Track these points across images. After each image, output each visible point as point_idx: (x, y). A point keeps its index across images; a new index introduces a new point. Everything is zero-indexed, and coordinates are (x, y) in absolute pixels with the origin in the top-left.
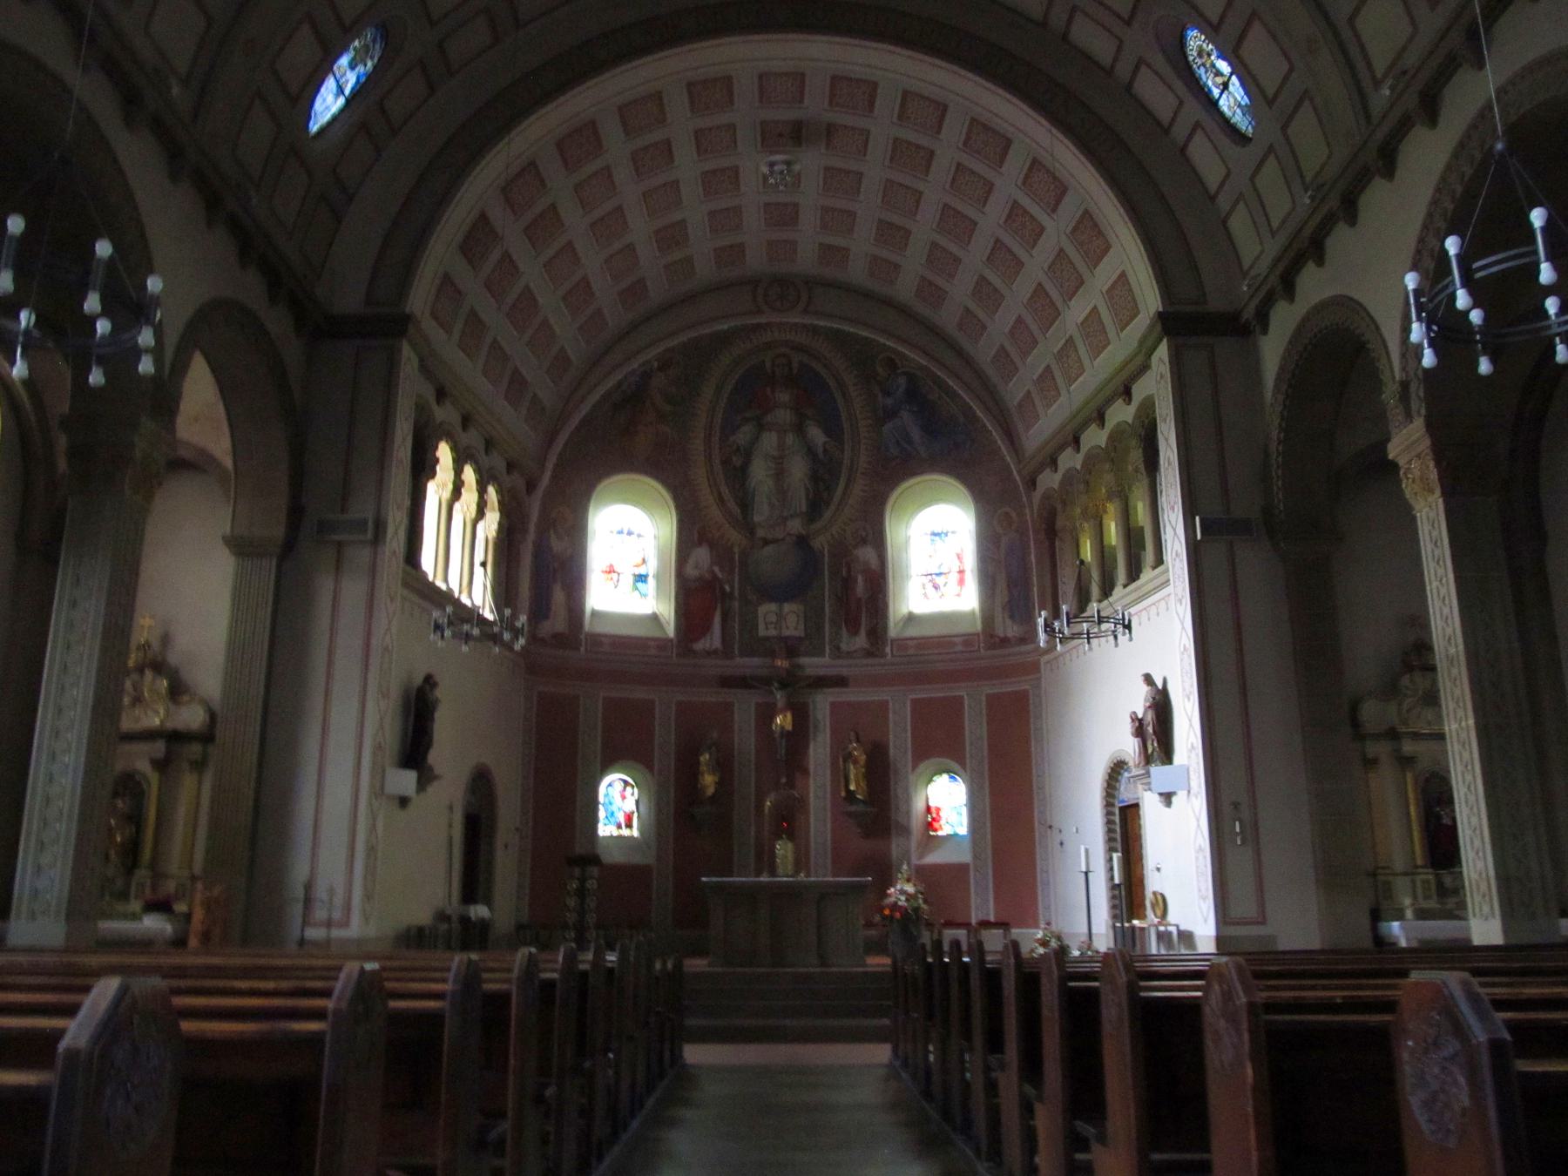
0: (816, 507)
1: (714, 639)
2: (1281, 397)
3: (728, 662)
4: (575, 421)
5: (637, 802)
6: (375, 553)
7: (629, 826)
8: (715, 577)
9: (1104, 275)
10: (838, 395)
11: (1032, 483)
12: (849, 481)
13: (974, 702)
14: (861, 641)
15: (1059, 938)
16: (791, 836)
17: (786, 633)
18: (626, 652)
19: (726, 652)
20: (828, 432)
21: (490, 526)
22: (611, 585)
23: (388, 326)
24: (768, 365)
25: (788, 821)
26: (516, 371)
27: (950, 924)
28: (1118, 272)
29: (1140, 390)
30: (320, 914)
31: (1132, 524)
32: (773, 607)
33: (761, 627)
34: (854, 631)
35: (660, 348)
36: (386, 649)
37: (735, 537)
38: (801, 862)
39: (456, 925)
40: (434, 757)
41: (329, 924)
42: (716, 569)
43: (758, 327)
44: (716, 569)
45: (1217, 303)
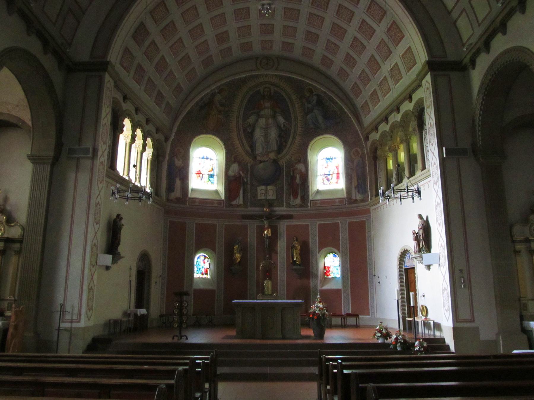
0: (280, 149)
1: (240, 200)
2: (481, 96)
3: (246, 209)
4: (184, 114)
5: (210, 264)
6: (93, 162)
7: (206, 274)
8: (241, 175)
9: (401, 49)
10: (290, 105)
11: (367, 138)
12: (294, 137)
13: (343, 227)
14: (298, 201)
15: (386, 329)
16: (270, 279)
17: (268, 198)
18: (205, 206)
19: (245, 205)
20: (285, 119)
21: (148, 154)
22: (200, 179)
23: (99, 66)
24: (262, 91)
25: (269, 273)
26: (159, 91)
27: (335, 315)
28: (408, 46)
29: (416, 97)
30: (68, 317)
31: (411, 153)
32: (263, 187)
33: (259, 195)
34: (295, 197)
35: (218, 84)
36: (98, 203)
37: (248, 159)
38: (275, 288)
39: (131, 318)
40: (121, 249)
41: (72, 321)
42: (241, 173)
43: (257, 76)
44: (241, 173)
45: (452, 57)
